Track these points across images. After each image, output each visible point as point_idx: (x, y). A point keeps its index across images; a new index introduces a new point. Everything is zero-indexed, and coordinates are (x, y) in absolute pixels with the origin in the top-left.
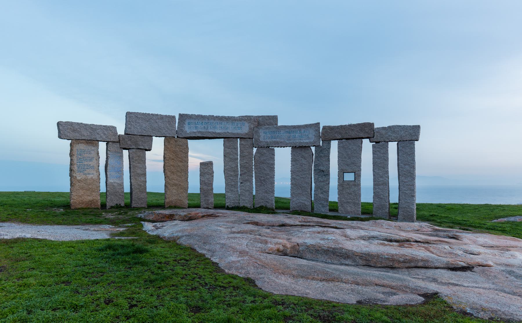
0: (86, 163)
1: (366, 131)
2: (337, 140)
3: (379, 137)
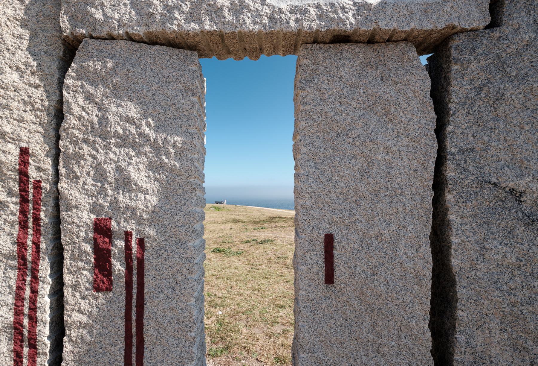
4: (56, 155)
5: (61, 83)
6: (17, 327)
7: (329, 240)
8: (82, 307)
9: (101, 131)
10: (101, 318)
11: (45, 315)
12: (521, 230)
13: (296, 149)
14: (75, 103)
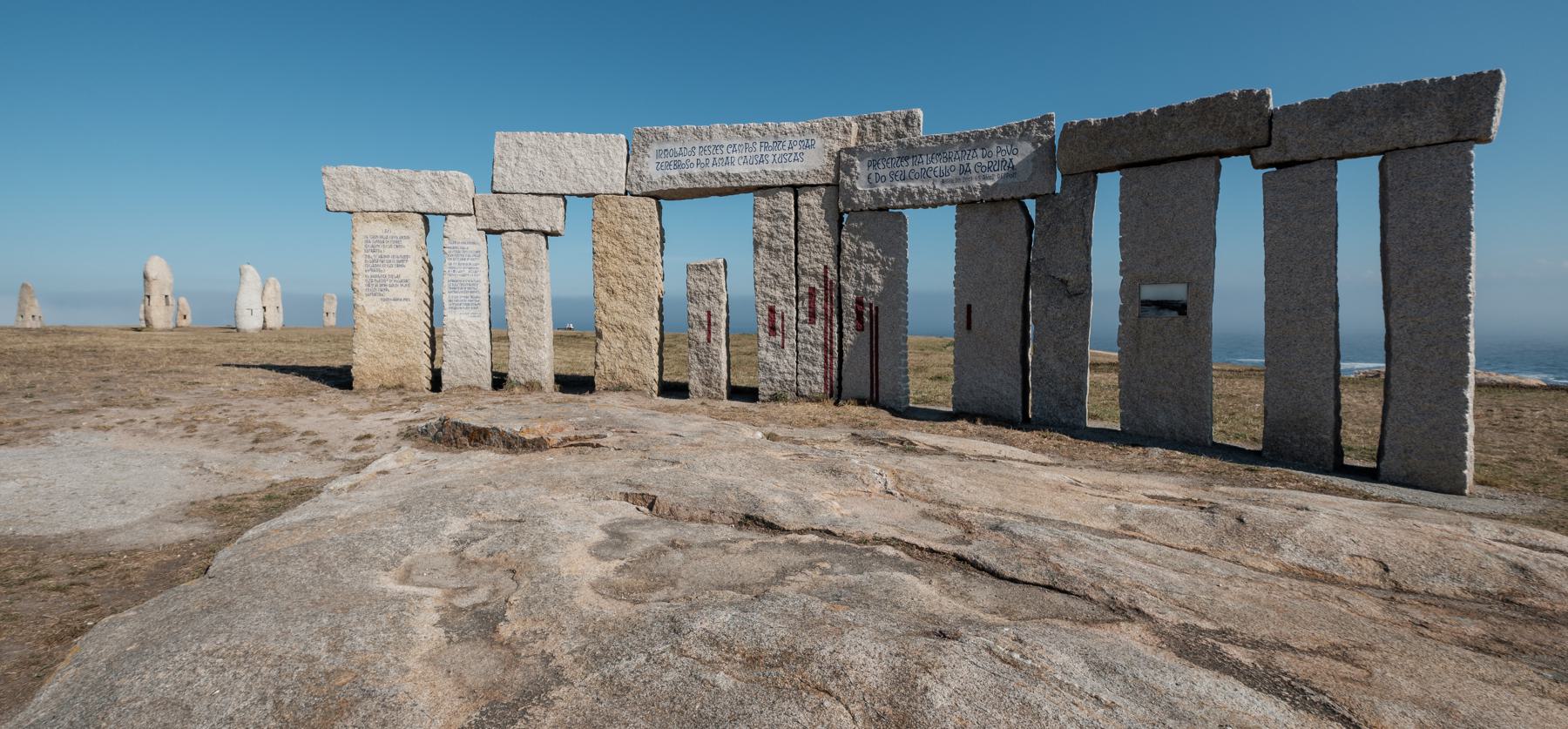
0: (388, 271)
1: (1240, 126)
2: (1119, 168)
3: (1294, 146)
4: (839, 267)
5: (840, 235)
6: (825, 345)
7: (969, 307)
8: (850, 337)
9: (858, 256)
10: (857, 341)
11: (836, 341)
12: (1066, 300)
13: (1086, 325)
14: (848, 245)
